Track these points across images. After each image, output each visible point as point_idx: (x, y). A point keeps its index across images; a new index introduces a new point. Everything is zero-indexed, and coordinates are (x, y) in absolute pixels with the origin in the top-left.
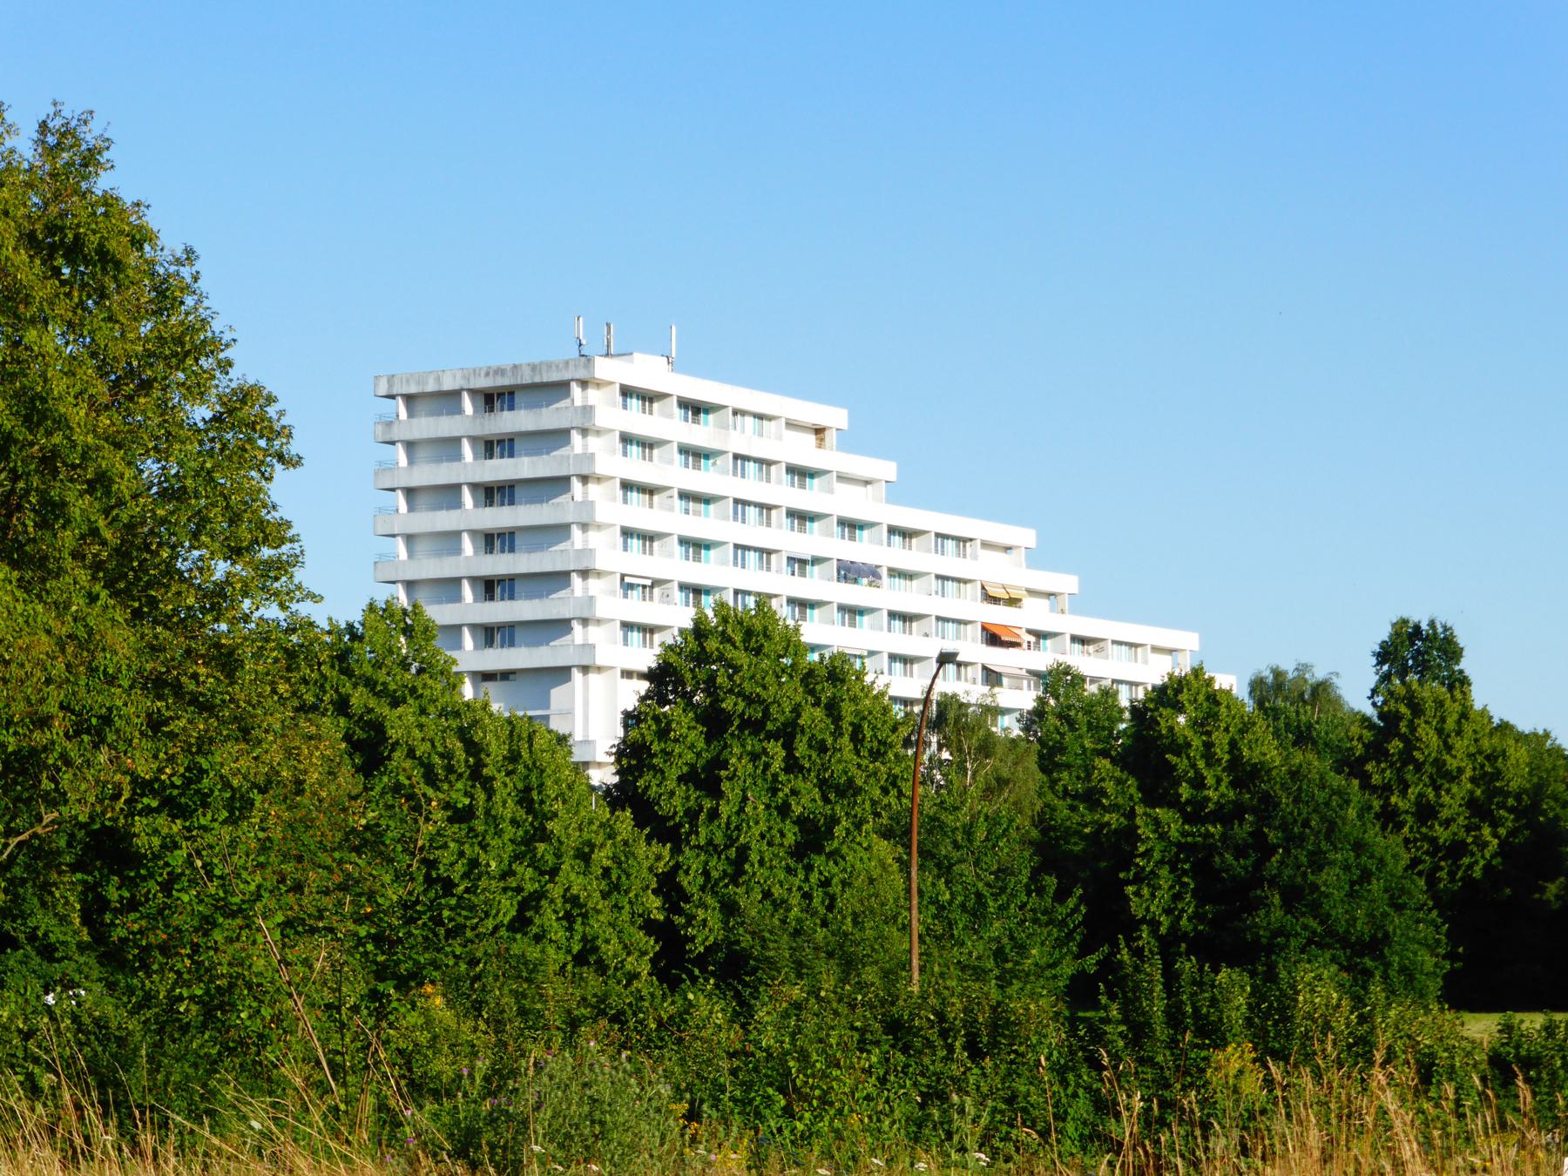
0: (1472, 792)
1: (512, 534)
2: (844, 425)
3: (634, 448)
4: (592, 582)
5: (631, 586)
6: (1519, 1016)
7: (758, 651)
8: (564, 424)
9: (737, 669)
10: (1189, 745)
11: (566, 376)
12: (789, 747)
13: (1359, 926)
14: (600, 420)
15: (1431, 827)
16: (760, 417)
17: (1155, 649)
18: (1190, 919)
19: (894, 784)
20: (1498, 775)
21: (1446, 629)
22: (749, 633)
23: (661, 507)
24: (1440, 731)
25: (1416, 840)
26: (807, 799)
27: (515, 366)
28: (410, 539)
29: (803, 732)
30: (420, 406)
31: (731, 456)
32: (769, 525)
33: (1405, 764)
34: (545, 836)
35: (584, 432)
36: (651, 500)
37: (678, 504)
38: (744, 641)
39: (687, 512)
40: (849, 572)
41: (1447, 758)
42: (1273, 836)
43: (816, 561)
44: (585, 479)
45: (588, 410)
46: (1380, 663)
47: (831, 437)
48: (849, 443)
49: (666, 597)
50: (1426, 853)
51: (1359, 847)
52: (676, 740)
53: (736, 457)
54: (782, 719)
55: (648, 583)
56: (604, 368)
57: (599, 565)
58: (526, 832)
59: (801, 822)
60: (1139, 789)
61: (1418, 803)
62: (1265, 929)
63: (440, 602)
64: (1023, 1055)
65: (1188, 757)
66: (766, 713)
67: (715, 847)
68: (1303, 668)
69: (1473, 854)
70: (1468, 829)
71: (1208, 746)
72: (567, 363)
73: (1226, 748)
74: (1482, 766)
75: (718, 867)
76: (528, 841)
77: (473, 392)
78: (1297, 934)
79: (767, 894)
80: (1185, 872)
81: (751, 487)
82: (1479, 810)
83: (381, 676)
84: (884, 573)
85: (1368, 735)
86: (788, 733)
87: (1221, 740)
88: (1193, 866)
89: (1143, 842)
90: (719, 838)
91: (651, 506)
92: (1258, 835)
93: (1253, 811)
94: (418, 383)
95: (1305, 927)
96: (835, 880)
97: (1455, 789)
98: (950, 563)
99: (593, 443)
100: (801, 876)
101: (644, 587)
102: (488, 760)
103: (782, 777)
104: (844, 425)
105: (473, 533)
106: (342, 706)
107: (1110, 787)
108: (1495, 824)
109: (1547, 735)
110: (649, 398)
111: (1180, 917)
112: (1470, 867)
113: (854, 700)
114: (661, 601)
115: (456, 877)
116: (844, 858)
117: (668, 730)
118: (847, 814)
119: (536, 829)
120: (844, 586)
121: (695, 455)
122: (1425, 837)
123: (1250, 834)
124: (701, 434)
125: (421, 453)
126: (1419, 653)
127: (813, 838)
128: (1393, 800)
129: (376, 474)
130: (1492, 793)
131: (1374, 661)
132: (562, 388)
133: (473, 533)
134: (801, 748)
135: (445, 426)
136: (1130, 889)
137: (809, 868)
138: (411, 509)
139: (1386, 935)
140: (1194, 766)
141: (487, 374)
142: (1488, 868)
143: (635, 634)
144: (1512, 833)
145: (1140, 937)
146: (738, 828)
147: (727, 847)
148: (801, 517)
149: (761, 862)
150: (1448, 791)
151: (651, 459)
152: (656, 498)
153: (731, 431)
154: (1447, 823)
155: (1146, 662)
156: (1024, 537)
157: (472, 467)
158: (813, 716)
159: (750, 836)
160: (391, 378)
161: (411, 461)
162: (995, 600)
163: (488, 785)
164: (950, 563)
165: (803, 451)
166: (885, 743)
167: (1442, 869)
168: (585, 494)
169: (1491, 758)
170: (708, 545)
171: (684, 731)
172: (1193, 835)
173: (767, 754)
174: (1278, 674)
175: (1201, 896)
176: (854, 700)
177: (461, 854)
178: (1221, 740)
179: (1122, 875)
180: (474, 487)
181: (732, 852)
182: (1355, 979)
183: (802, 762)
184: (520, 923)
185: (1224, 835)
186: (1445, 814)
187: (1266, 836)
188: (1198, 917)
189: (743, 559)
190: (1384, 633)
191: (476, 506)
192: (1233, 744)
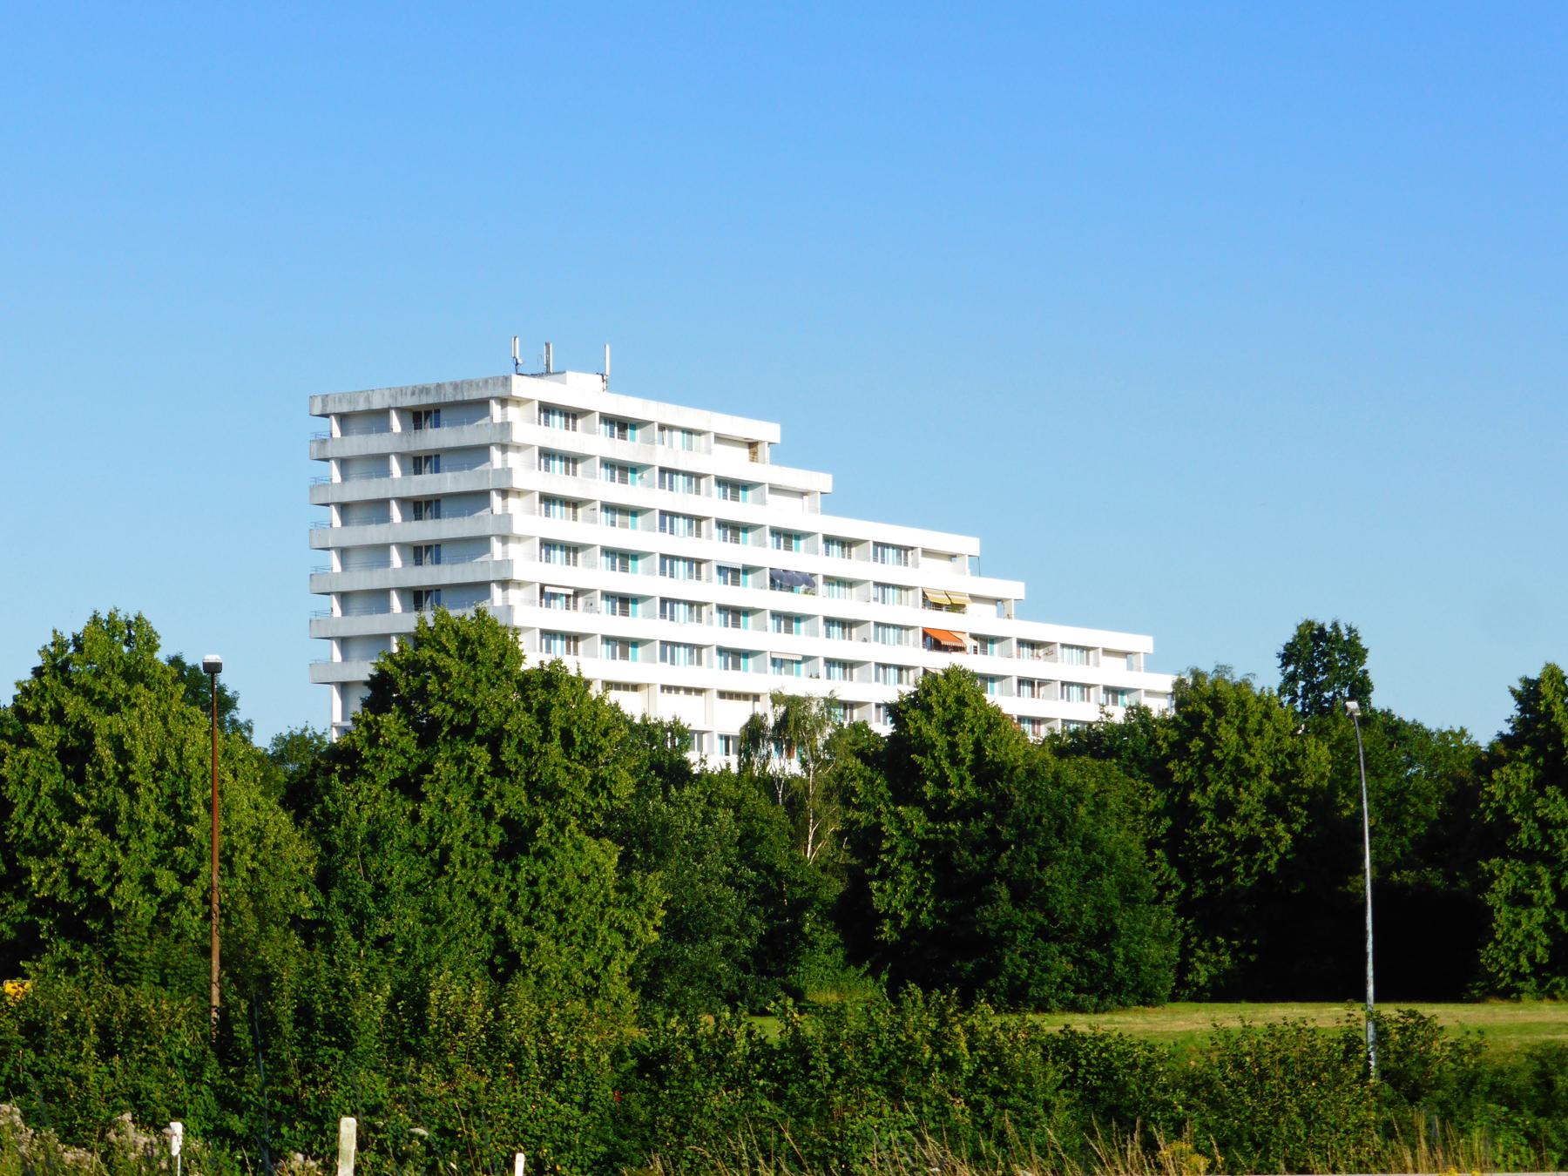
0: (1271, 789)
1: (438, 546)
2: (777, 439)
3: (557, 463)
4: (513, 593)
5: (554, 596)
6: (1426, 1010)
7: (472, 659)
8: (484, 441)
9: (448, 676)
10: (934, 746)
11: (485, 394)
12: (495, 750)
13: (1085, 919)
14: (518, 436)
15: (1229, 824)
16: (689, 432)
17: (1107, 652)
18: (929, 913)
19: (603, 787)
20: (1297, 772)
21: (1350, 630)
22: (465, 641)
23: (585, 519)
24: (1241, 731)
25: (1214, 836)
26: (515, 798)
27: (439, 386)
28: (344, 552)
29: (510, 736)
30: (354, 424)
31: (657, 470)
32: (699, 535)
33: (1205, 763)
34: (186, 840)
35: (504, 448)
36: (575, 513)
37: (603, 516)
38: (458, 649)
40: (781, 580)
41: (1245, 756)
42: (1006, 833)
43: (747, 570)
44: (504, 493)
45: (506, 426)
46: (1285, 664)
47: (765, 451)
48: (782, 456)
49: (590, 606)
50: (1224, 848)
51: (1089, 844)
52: (387, 746)
53: (663, 470)
54: (491, 724)
55: (571, 592)
56: (521, 386)
57: (517, 576)
58: (170, 836)
59: (505, 822)
60: (889, 787)
62: (994, 922)
63: (370, 613)
64: (155, 1053)
65: (933, 757)
66: (474, 717)
67: (418, 848)
68: (1221, 670)
69: (1267, 850)
70: (1264, 824)
71: (953, 746)
72: (486, 382)
73: (971, 747)
74: (1283, 764)
76: (169, 845)
77: (401, 411)
78: (1023, 929)
79: (472, 894)
80: (927, 868)
81: (679, 499)
82: (1274, 806)
83: (99, 686)
84: (820, 580)
85: (1174, 735)
86: (494, 742)
87: (965, 741)
88: (935, 861)
89: (887, 838)
90: (422, 840)
91: (575, 518)
92: (992, 831)
93: (992, 809)
94: (350, 402)
95: (1031, 921)
96: (542, 880)
97: (1254, 786)
98: (890, 571)
99: (513, 458)
100: (508, 875)
101: (568, 596)
102: (134, 767)
103: (488, 780)
104: (777, 439)
105: (402, 546)
106: (58, 715)
107: (859, 785)
108: (1289, 820)
109: (1463, 732)
110: (572, 415)
111: (920, 911)
112: (1265, 861)
113: (564, 705)
114: (585, 610)
115: (97, 880)
116: (552, 858)
117: (378, 735)
118: (551, 816)
119: (179, 834)
120: (777, 593)
121: (622, 469)
122: (1223, 833)
123: (987, 831)
124: (625, 449)
125: (355, 469)
126: (1323, 657)
127: (517, 840)
128: (1193, 797)
129: (312, 489)
130: (1289, 790)
131: (1279, 662)
133: (402, 546)
134: (509, 752)
135: (373, 443)
136: (874, 884)
137: (516, 869)
138: (345, 523)
139: (1114, 928)
140: (938, 766)
141: (413, 393)
142: (1282, 863)
143: (559, 642)
144: (1306, 829)
145: (882, 932)
146: (441, 830)
147: (430, 848)
148: (734, 529)
149: (463, 864)
150: (1247, 788)
151: (575, 474)
152: (580, 510)
153: (659, 447)
154: (1245, 819)
155: (1097, 664)
156: (969, 545)
157: (399, 481)
158: (523, 722)
159: (453, 837)
160: (325, 398)
162: (938, 606)
163: (131, 790)
164: (890, 571)
165: (736, 464)
166: (594, 747)
167: (1238, 863)
168: (505, 507)
169: (1291, 756)
170: (635, 556)
171: (395, 736)
172: (935, 831)
173: (470, 759)
174: (1197, 675)
175: (940, 892)
176: (564, 705)
177: (103, 858)
178: (965, 741)
179: (867, 871)
180: (402, 501)
181: (436, 853)
182: (1082, 972)
183: (508, 765)
184: (160, 924)
185: (962, 832)
186: (1242, 810)
187: (999, 833)
188: (937, 911)
189: (672, 568)
190: (1288, 634)
191: (404, 519)
192: (978, 748)
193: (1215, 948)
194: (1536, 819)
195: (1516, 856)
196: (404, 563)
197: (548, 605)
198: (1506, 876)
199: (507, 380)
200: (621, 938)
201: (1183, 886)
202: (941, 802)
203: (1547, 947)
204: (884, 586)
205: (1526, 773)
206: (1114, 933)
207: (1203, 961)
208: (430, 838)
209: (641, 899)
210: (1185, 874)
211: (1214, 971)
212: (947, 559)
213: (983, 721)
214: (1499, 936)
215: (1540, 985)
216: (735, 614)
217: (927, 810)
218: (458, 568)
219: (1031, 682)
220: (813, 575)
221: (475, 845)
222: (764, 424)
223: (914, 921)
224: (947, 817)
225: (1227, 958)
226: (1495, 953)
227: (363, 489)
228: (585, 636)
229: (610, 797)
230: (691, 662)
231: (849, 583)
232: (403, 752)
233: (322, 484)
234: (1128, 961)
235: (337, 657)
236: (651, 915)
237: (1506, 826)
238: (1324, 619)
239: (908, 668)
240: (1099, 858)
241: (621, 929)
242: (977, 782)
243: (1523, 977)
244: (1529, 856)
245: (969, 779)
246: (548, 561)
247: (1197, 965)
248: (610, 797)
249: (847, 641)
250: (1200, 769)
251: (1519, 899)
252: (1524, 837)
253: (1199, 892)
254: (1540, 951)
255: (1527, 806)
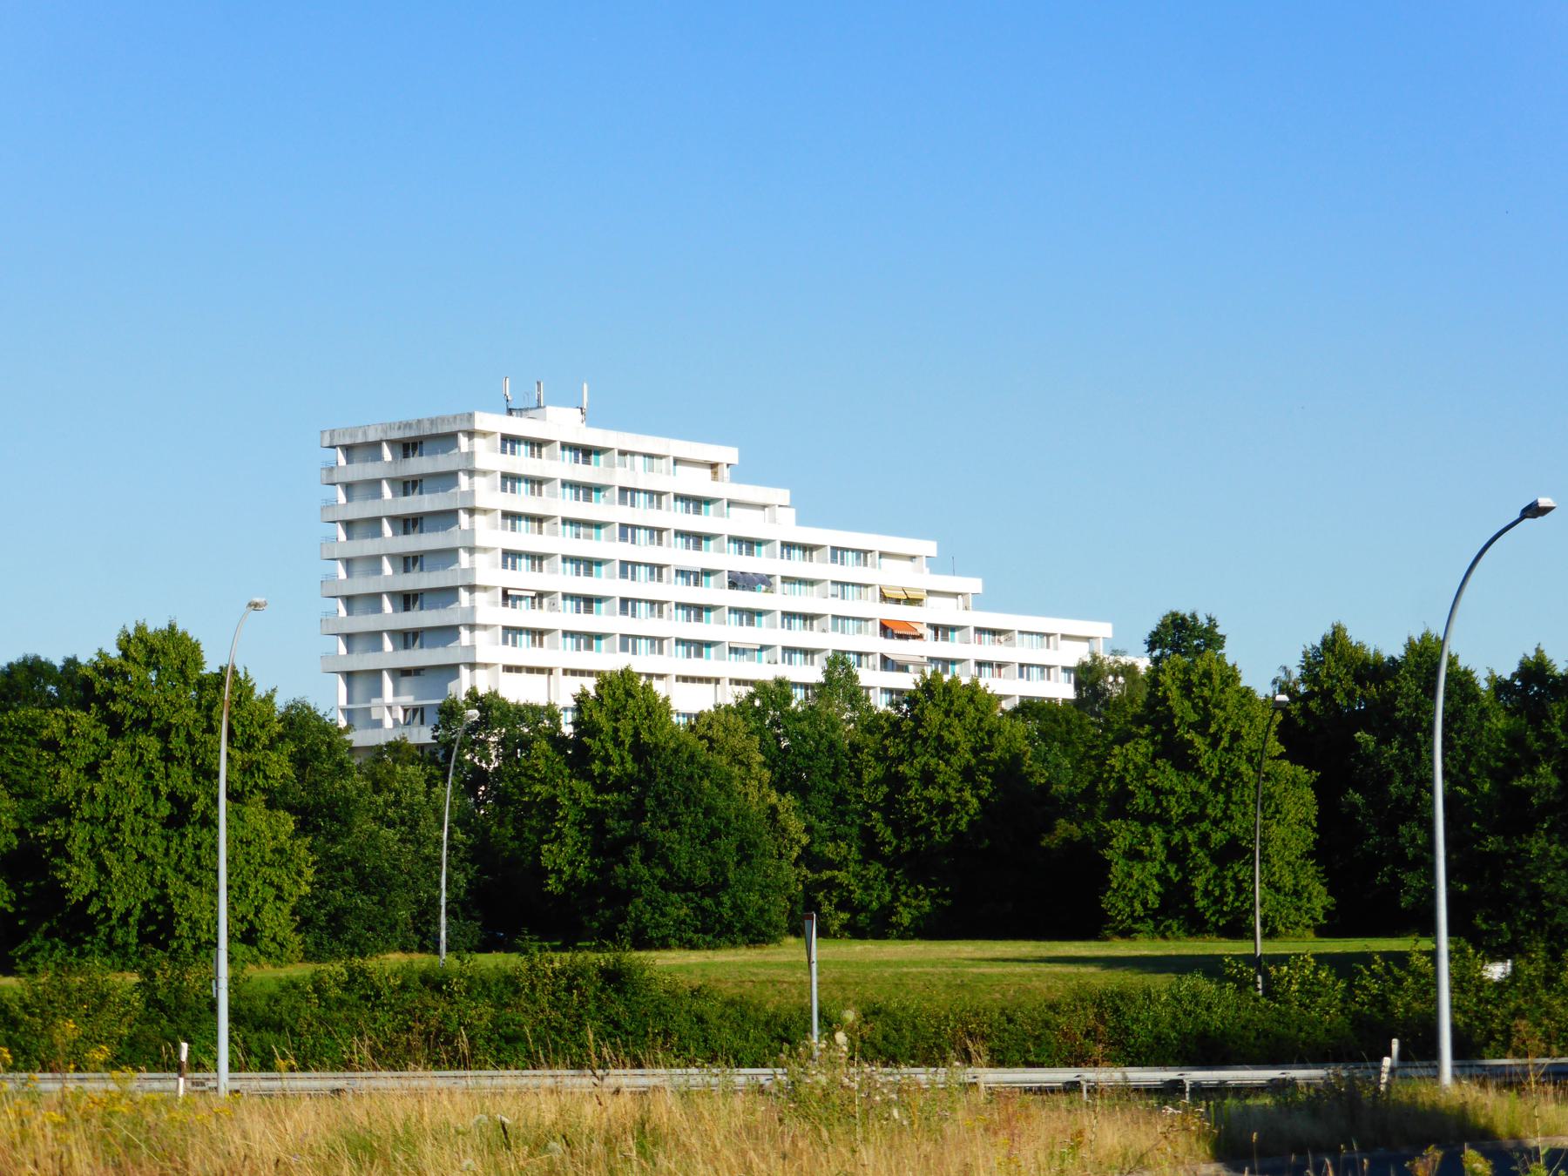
2: (735, 460)
8: (452, 467)
11: (454, 428)
16: (651, 456)
17: (1064, 637)
26: (182, 777)
30: (357, 454)
36: (540, 527)
39: (578, 536)
43: (708, 573)
47: (725, 472)
48: (740, 474)
59: (172, 797)
61: (923, 771)
71: (616, 730)
73: (631, 732)
75: (101, 834)
77: (392, 443)
81: (641, 514)
84: (778, 579)
87: (626, 727)
91: (540, 532)
97: (953, 759)
98: (850, 571)
108: (977, 786)
131: (1146, 648)
132: (453, 436)
134: (177, 742)
137: (183, 836)
142: (971, 824)
148: (697, 539)
149: (133, 832)
154: (943, 787)
155: (1056, 648)
156: (928, 548)
157: (390, 501)
159: (126, 808)
161: (349, 498)
165: (697, 482)
167: (934, 824)
178: (626, 727)
190: (1152, 624)
193: (916, 895)
194: (1148, 787)
195: (1135, 818)
196: (395, 571)
197: (514, 606)
198: (1123, 834)
199: (471, 416)
200: (273, 891)
201: (895, 842)
202: (604, 775)
203: (1159, 894)
204: (844, 584)
205: (1145, 747)
206: (725, 885)
207: (906, 905)
208: (107, 811)
209: (290, 860)
210: (897, 834)
211: (915, 913)
212: (907, 563)
213: (643, 710)
214: (1114, 885)
215: (1157, 927)
216: (699, 611)
217: (594, 784)
218: (434, 575)
219: (990, 664)
220: (770, 576)
221: (146, 816)
222: (723, 448)
223: (573, 875)
224: (608, 790)
225: (927, 902)
226: (1113, 900)
227: (362, 509)
228: (549, 631)
229: (266, 777)
230: (653, 652)
231: (811, 583)
232: (96, 741)
233: (331, 505)
234: (734, 907)
235: (343, 650)
236: (300, 873)
237: (1124, 795)
238: (1185, 610)
239: (867, 654)
240: (716, 822)
241: (271, 884)
242: (635, 760)
243: (1137, 920)
244: (1145, 819)
245: (629, 758)
246: (514, 568)
247: (901, 909)
248: (266, 777)
249: (537, 649)
250: (910, 744)
251: (1134, 855)
252: (1141, 802)
253: (907, 848)
254: (1151, 897)
255: (1141, 777)
